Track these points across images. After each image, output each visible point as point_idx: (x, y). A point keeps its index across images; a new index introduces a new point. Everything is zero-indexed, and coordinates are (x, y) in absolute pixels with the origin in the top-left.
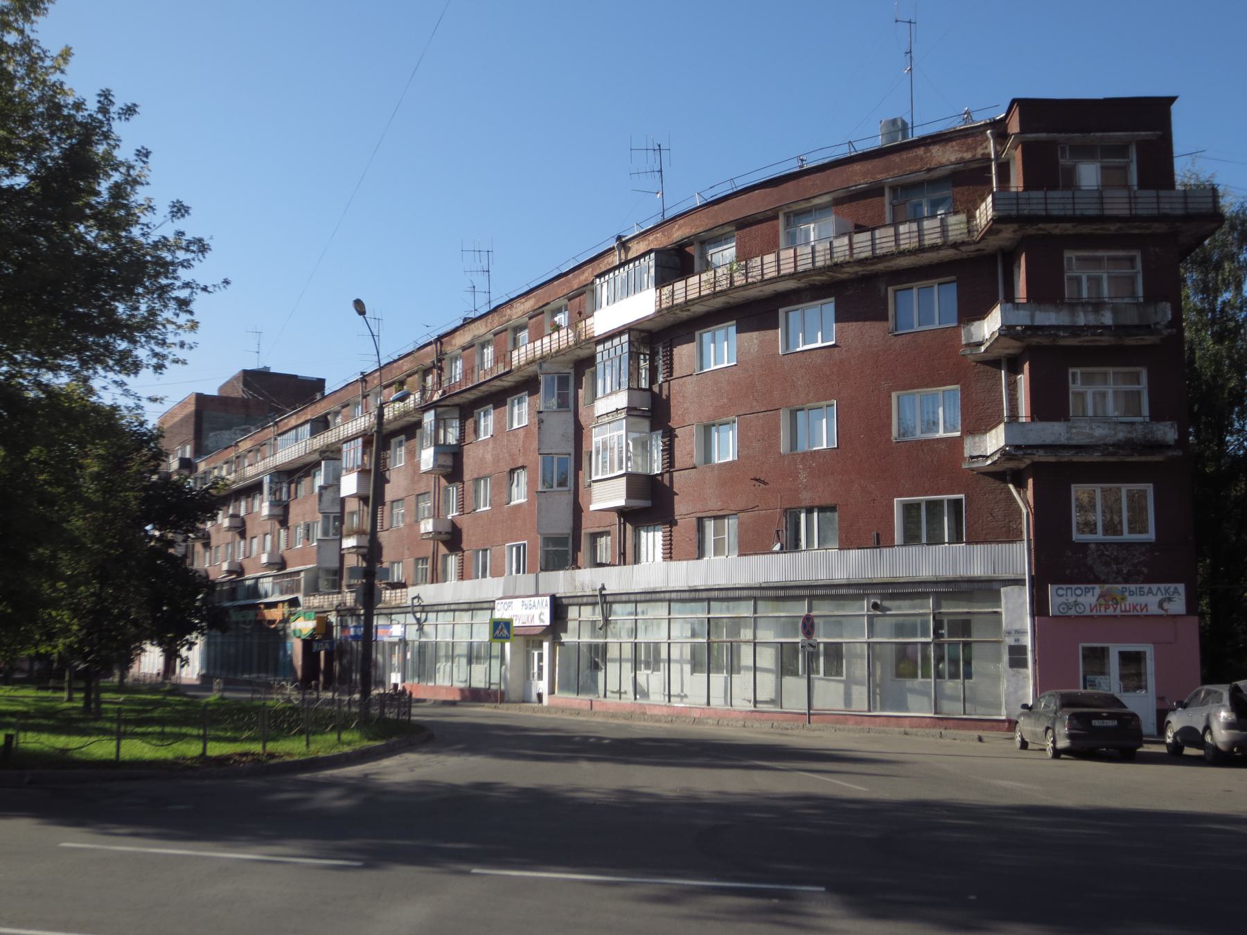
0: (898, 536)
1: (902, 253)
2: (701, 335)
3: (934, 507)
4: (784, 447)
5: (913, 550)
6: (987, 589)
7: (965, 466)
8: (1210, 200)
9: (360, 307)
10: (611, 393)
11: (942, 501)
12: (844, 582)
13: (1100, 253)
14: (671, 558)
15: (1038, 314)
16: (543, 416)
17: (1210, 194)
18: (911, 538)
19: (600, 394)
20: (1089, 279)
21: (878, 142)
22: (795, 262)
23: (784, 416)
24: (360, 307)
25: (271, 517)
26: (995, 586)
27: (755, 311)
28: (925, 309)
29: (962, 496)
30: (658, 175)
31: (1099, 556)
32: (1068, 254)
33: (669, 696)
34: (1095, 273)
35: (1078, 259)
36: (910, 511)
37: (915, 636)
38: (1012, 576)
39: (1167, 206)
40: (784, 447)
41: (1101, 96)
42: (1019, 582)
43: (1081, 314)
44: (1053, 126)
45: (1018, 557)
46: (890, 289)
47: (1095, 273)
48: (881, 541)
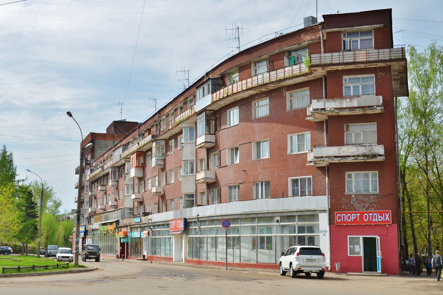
0: (290, 193)
1: (273, 83)
2: (230, 112)
3: (303, 180)
4: (254, 157)
5: (296, 198)
6: (313, 215)
7: (307, 165)
8: (401, 52)
9: (69, 114)
10: (200, 136)
11: (305, 178)
12: (220, 215)
13: (359, 76)
14: (221, 202)
15: (327, 103)
16: (187, 73)
17: (401, 50)
18: (295, 194)
19: (198, 136)
20: (354, 87)
21: (302, 27)
22: (270, 78)
23: (254, 146)
24: (69, 114)
25: (113, 186)
26: (317, 213)
27: (245, 103)
28: (300, 100)
29: (311, 176)
30: (238, 39)
31: (356, 200)
32: (345, 77)
33: (239, 38)
34: (356, 85)
35: (349, 79)
36: (295, 182)
37: (304, 232)
38: (323, 209)
39: (382, 56)
40: (254, 157)
41: (359, 11)
42: (324, 211)
43: (345, 103)
44: (338, 24)
45: (322, 202)
46: (287, 93)
47: (356, 85)
48: (284, 195)
